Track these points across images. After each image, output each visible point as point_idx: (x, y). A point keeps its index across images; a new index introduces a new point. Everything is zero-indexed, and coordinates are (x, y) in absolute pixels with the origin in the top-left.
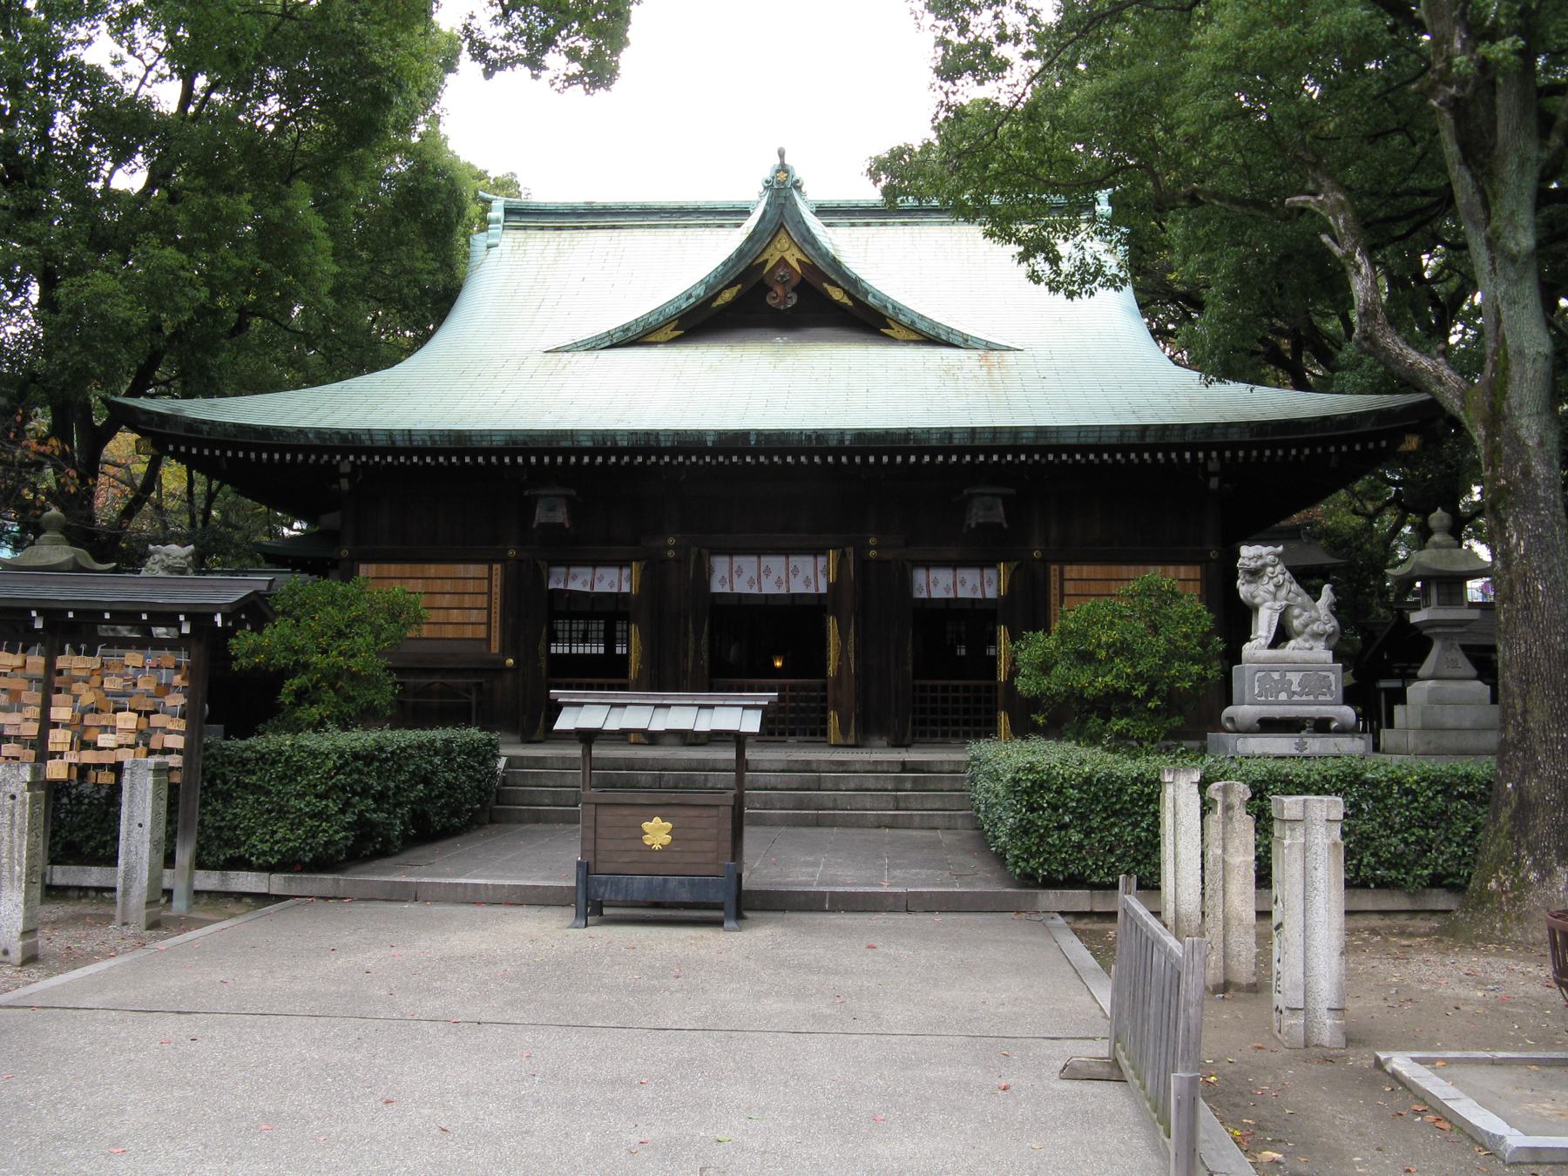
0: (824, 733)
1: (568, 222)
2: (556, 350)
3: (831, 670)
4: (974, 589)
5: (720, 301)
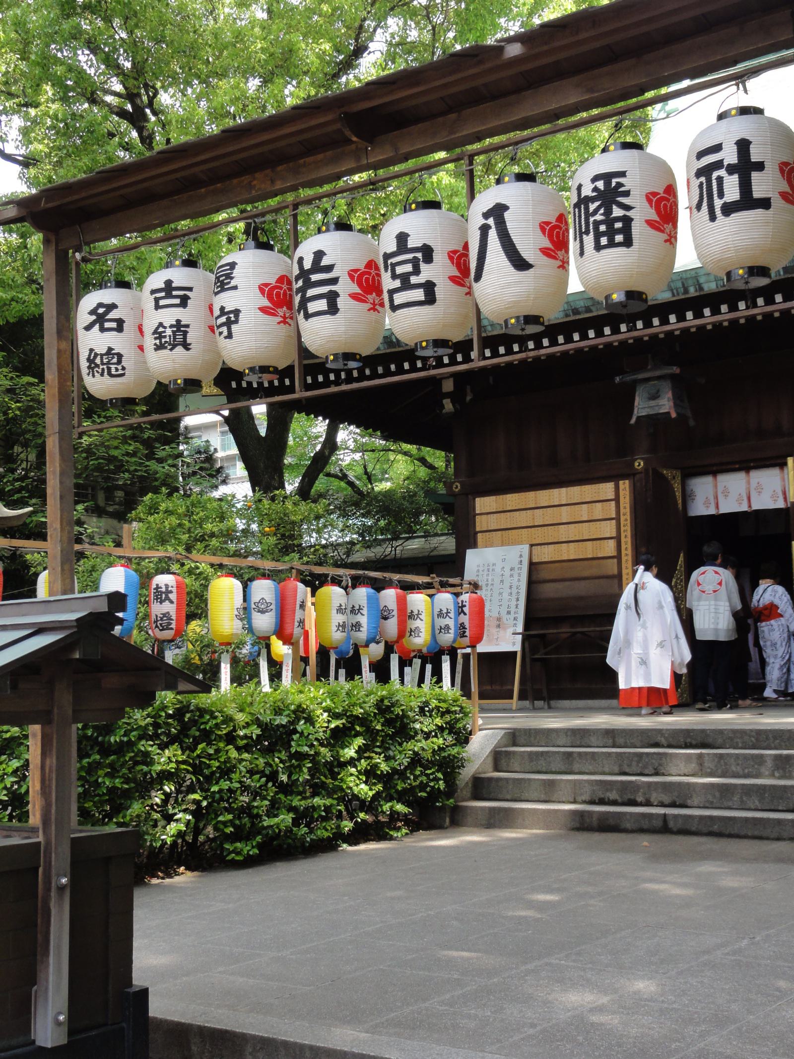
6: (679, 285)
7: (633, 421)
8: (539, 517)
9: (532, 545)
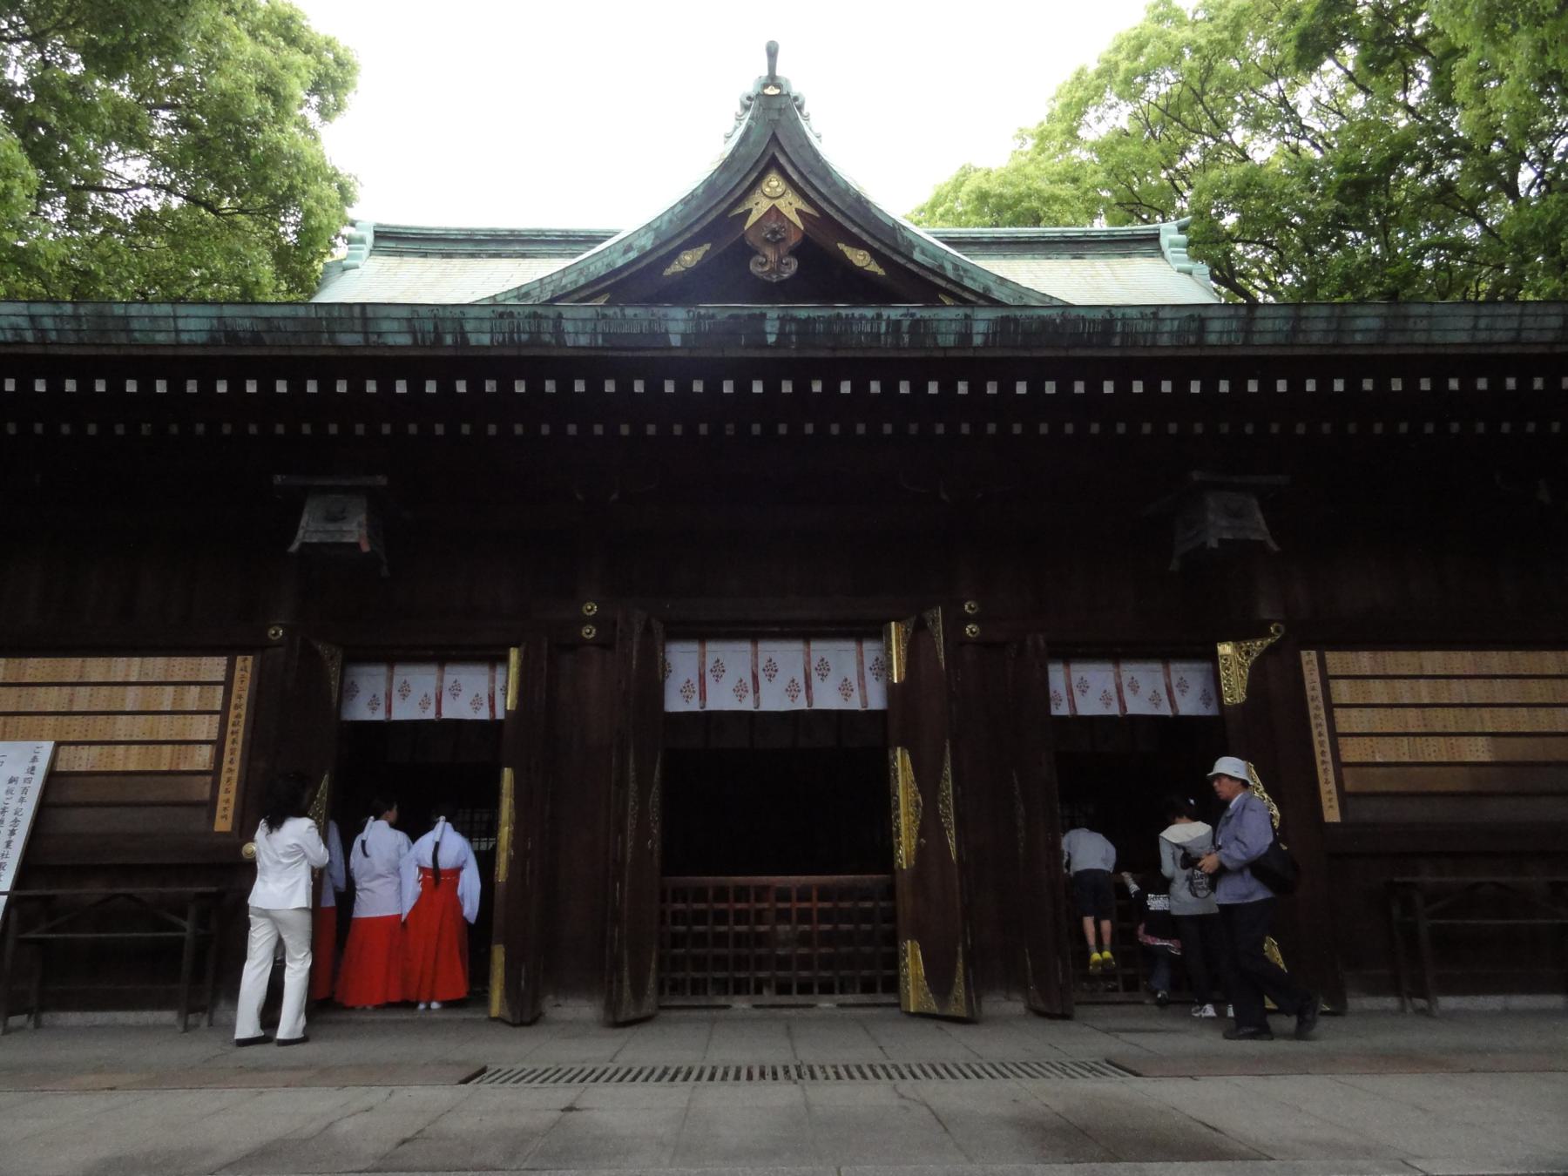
0: (892, 985)
3: (905, 850)
6: (429, 326)
7: (294, 547)
8: (83, 699)
9: (58, 744)
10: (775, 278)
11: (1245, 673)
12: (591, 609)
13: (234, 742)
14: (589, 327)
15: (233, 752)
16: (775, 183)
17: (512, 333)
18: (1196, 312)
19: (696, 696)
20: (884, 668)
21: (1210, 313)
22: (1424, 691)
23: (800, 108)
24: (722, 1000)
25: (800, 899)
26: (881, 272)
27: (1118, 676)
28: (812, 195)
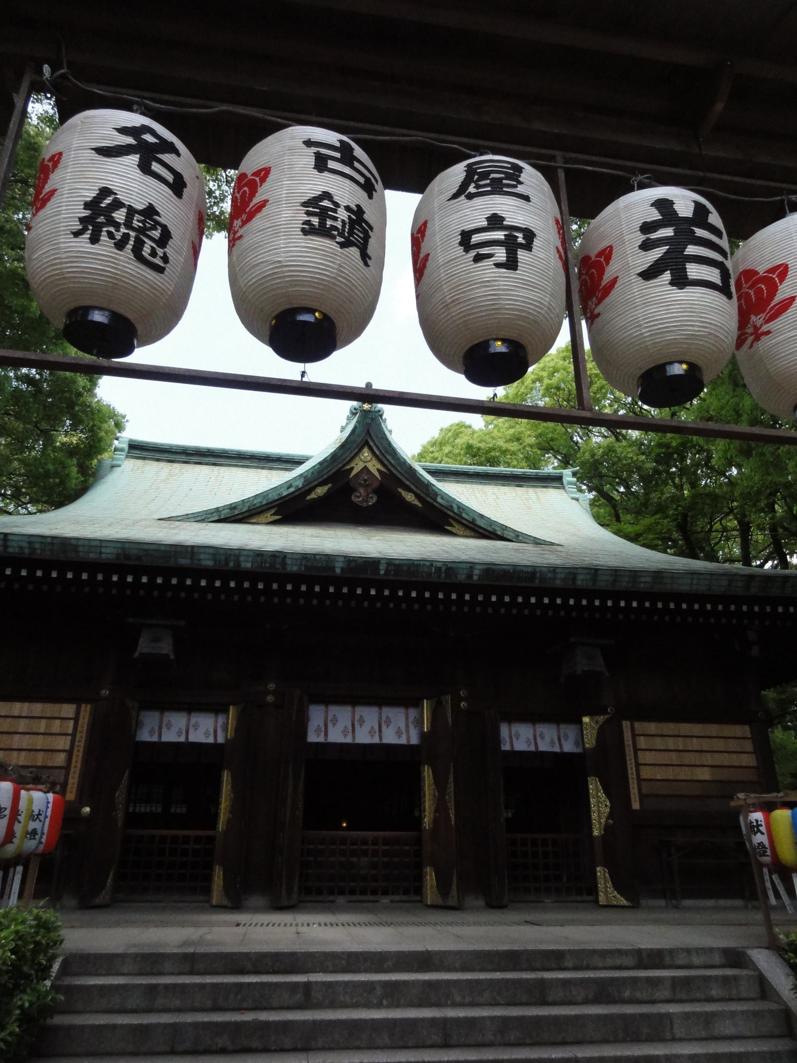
0: (419, 890)
1: (178, 457)
2: (169, 519)
3: (427, 821)
4: (552, 743)
5: (313, 496)
6: (223, 558)
7: (136, 655)
10: (365, 505)
11: (595, 732)
12: (272, 686)
13: (78, 751)
14: (299, 562)
15: (77, 756)
16: (366, 454)
17: (261, 563)
18: (572, 570)
19: (323, 734)
20: (419, 722)
21: (579, 571)
22: (680, 744)
23: (381, 416)
24: (331, 898)
25: (373, 844)
26: (420, 505)
27: (535, 731)
28: (386, 463)
